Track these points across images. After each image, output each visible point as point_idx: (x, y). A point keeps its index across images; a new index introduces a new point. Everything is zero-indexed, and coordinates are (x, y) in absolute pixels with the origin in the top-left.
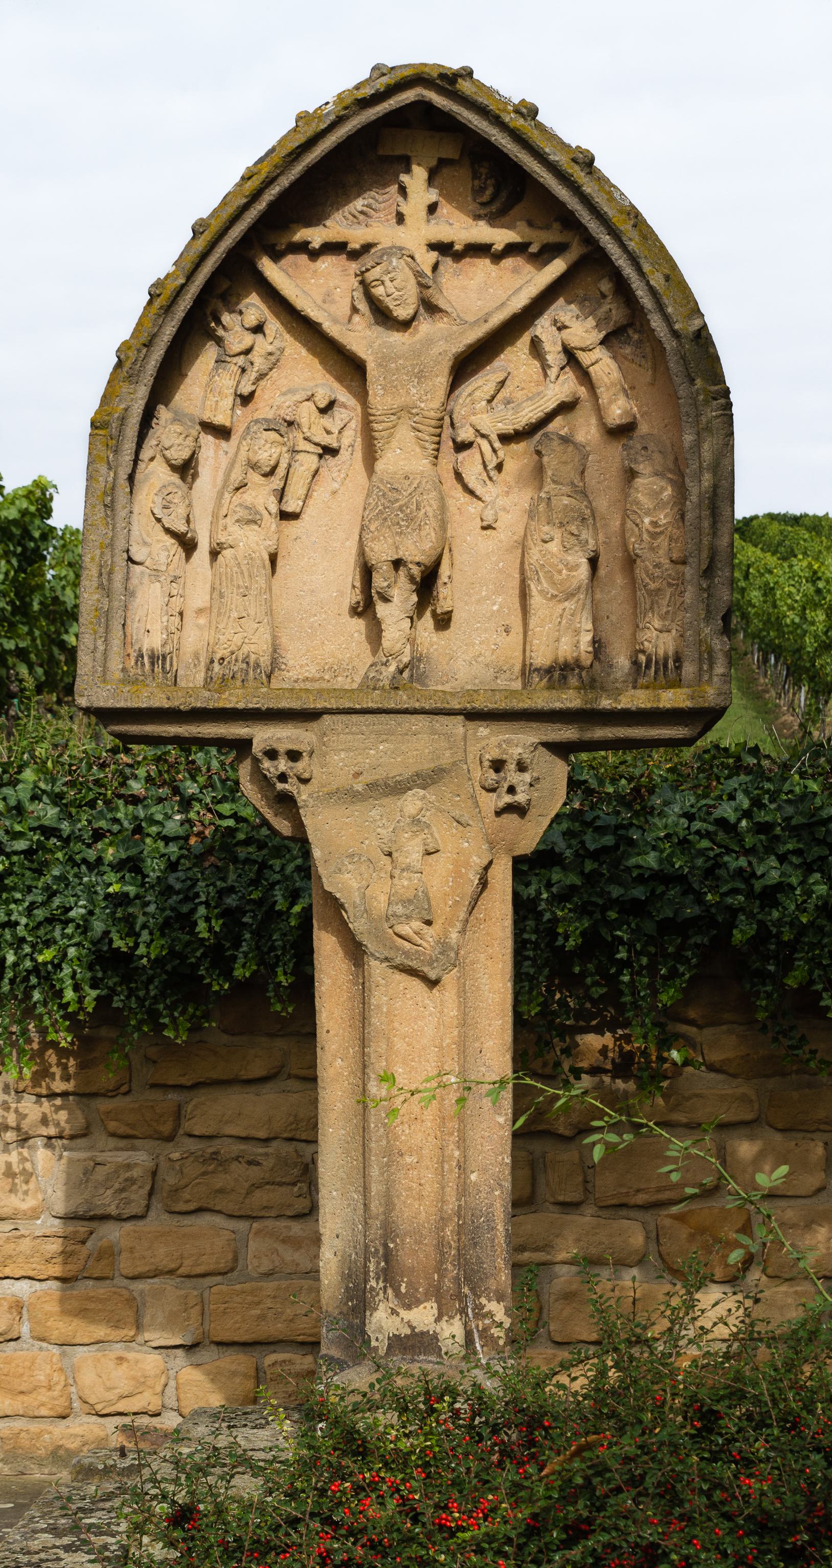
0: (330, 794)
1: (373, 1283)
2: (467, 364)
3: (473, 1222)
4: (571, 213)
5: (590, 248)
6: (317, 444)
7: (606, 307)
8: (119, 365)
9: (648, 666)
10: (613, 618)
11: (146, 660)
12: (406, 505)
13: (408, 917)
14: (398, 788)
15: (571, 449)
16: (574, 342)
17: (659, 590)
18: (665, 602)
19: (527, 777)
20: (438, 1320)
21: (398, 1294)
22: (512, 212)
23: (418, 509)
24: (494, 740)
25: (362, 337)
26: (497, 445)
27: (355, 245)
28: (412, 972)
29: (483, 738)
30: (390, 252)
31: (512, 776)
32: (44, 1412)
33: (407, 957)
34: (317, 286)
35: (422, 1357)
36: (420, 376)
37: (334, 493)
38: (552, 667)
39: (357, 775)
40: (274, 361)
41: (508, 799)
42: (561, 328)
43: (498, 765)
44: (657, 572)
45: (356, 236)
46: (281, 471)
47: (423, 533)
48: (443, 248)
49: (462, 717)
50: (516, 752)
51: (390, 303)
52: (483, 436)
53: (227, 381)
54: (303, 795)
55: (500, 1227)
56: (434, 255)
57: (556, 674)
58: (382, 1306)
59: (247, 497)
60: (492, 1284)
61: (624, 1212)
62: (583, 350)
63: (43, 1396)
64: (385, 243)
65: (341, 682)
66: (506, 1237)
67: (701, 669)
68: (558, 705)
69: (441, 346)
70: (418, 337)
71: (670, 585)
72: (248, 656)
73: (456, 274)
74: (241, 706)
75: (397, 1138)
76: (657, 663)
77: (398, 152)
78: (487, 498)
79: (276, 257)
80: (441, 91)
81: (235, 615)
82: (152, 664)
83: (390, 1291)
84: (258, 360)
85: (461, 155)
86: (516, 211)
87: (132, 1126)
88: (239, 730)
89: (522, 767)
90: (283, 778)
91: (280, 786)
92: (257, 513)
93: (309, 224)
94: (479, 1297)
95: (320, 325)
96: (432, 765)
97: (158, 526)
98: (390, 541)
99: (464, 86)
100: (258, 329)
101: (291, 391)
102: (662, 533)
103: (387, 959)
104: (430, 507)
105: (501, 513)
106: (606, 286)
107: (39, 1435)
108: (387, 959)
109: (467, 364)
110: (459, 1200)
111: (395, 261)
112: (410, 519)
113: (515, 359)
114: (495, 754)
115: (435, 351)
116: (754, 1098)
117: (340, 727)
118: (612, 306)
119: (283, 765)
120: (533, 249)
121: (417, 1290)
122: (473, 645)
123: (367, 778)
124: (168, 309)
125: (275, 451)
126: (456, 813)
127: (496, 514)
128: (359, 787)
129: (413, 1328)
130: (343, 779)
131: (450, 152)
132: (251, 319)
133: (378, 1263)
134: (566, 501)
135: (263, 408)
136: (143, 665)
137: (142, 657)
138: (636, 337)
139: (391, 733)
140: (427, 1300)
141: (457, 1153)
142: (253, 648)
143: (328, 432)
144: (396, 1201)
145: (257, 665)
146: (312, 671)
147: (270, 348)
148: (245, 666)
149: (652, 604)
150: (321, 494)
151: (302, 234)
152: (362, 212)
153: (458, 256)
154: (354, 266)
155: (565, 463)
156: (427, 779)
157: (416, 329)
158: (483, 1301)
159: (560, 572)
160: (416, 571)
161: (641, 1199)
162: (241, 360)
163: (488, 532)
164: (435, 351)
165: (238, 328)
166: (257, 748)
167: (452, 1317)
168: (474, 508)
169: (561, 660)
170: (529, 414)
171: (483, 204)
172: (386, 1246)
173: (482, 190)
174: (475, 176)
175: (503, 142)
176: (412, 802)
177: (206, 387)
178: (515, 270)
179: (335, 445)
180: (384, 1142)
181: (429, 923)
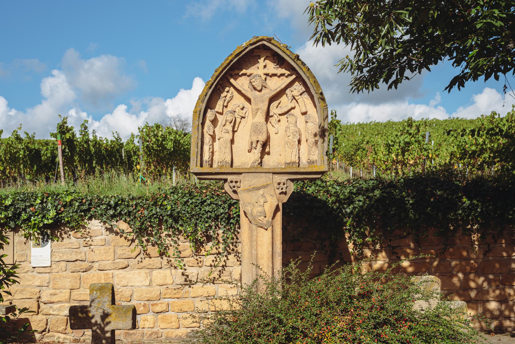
0: (244, 190)
2: (272, 100)
8: (199, 99)
14: (259, 189)
16: (294, 95)
19: (285, 186)
24: (278, 178)
25: (250, 94)
27: (248, 74)
28: (261, 227)
30: (256, 76)
31: (282, 185)
32: (174, 327)
34: (242, 83)
36: (263, 102)
40: (232, 98)
43: (279, 184)
45: (248, 72)
48: (267, 75)
50: (283, 181)
51: (256, 86)
54: (238, 190)
56: (265, 76)
59: (226, 127)
63: (173, 324)
64: (255, 74)
65: (245, 166)
68: (292, 171)
69: (267, 95)
73: (270, 80)
84: (228, 98)
86: (283, 66)
87: (193, 264)
90: (234, 187)
99: (273, 42)
100: (228, 92)
104: (265, 129)
107: (173, 332)
109: (272, 100)
113: (284, 99)
114: (279, 181)
120: (286, 75)
124: (210, 88)
126: (271, 194)
130: (247, 187)
135: (230, 108)
139: (257, 177)
146: (239, 164)
153: (271, 76)
154: (248, 78)
156: (264, 187)
160: (262, 143)
162: (224, 98)
164: (266, 96)
166: (229, 180)
168: (273, 129)
170: (285, 110)
176: (261, 192)
178: (282, 79)
181: (265, 217)
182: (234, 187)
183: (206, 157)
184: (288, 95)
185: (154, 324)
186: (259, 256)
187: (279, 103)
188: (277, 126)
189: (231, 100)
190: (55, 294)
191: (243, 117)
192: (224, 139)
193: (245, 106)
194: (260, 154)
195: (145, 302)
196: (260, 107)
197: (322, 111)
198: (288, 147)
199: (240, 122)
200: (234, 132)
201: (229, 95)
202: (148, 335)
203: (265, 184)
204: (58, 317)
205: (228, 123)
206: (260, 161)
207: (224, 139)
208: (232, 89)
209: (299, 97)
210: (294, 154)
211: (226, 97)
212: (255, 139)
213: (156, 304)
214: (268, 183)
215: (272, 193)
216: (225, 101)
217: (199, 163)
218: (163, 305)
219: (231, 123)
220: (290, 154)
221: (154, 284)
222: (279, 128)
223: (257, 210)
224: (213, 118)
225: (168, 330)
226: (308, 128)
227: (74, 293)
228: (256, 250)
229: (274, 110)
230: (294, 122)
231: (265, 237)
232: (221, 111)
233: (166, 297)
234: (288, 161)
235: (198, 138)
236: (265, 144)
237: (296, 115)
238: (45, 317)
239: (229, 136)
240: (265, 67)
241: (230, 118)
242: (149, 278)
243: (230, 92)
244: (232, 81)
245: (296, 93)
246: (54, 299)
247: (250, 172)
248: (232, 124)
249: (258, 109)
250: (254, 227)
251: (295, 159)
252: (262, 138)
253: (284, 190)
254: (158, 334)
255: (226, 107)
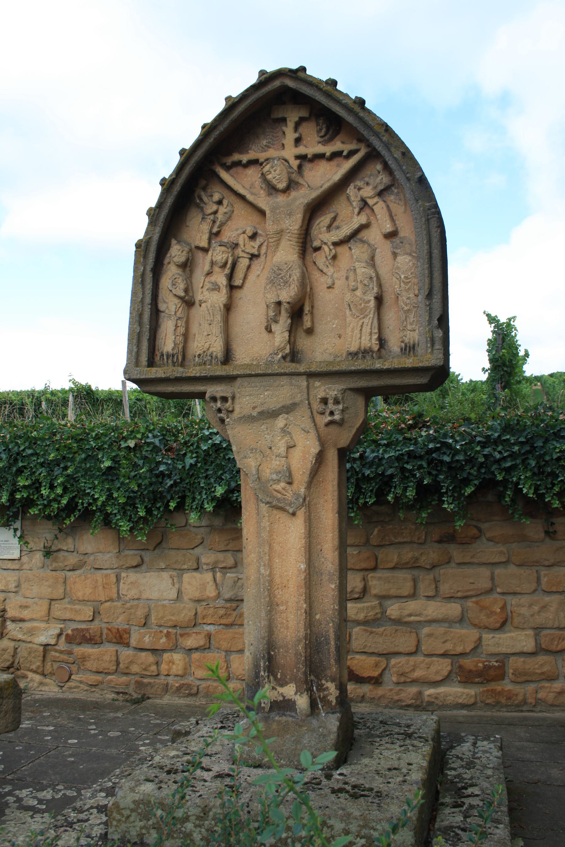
0: (240, 418)
1: (262, 673)
2: (315, 209)
3: (317, 640)
4: (356, 128)
5: (370, 149)
6: (248, 253)
7: (380, 178)
9: (405, 349)
10: (391, 328)
11: (165, 357)
12: (284, 276)
13: (279, 481)
14: (273, 414)
15: (366, 246)
17: (409, 310)
18: (412, 316)
19: (341, 407)
20: (296, 694)
21: (276, 678)
22: (335, 140)
23: (290, 277)
25: (263, 202)
26: (332, 247)
29: (317, 387)
33: (279, 502)
34: (245, 182)
35: (288, 713)
37: (258, 276)
38: (357, 352)
39: (254, 408)
41: (329, 418)
42: (359, 189)
43: (325, 401)
44: (408, 301)
45: (262, 156)
46: (229, 265)
47: (291, 288)
48: (302, 158)
49: (305, 377)
51: (275, 182)
52: (325, 244)
53: (205, 227)
55: (332, 643)
56: (298, 162)
57: (360, 355)
58: (267, 686)
59: (213, 278)
60: (329, 673)
61: (452, 600)
62: (370, 198)
66: (336, 648)
67: (427, 346)
69: (302, 200)
70: (290, 198)
71: (414, 307)
72: (212, 353)
73: (310, 170)
74: (198, 375)
75: (275, 596)
76: (410, 347)
77: (280, 116)
78: (329, 274)
79: (228, 168)
80: (291, 77)
81: (206, 334)
82: (168, 359)
83: (271, 678)
84: (220, 216)
85: (310, 115)
88: (199, 388)
89: (337, 402)
90: (219, 411)
91: (219, 415)
92: (217, 285)
93: (241, 153)
94: (321, 680)
95: (245, 196)
96: (291, 402)
97: (171, 294)
98: (275, 293)
100: (220, 203)
101: (237, 230)
102: (410, 282)
103: (268, 503)
105: (336, 281)
106: (379, 167)
108: (268, 503)
110: (306, 630)
111: (276, 162)
112: (286, 282)
115: (298, 203)
116: (506, 552)
117: (246, 384)
118: (383, 176)
119: (219, 404)
120: (345, 153)
121: (286, 677)
122: (324, 344)
123: (259, 410)
125: (225, 256)
126: (303, 426)
127: (334, 281)
128: (255, 414)
129: (284, 697)
130: (247, 411)
131: (304, 113)
132: (216, 197)
133: (265, 663)
134: (363, 270)
136: (163, 359)
137: (163, 355)
138: (396, 191)
140: (290, 683)
141: (305, 606)
142: (214, 349)
143: (254, 247)
144: (275, 629)
145: (216, 357)
146: (247, 361)
147: (225, 210)
148: (210, 358)
149: (406, 317)
150: (252, 277)
151: (236, 157)
152: (266, 146)
155: (363, 253)
156: (288, 409)
157: (289, 194)
158: (323, 682)
159: (361, 304)
161: (459, 594)
162: (212, 217)
163: (330, 290)
164: (298, 203)
165: (211, 203)
167: (302, 693)
168: (323, 279)
169: (362, 348)
170: (346, 231)
171: (322, 137)
172: (269, 653)
173: (321, 130)
174: (318, 125)
175: (322, 98)
176: (280, 422)
177: (197, 231)
179: (256, 253)
180: (268, 599)
181: (290, 483)
182: (219, 411)
183: (168, 341)
184: (352, 198)
185: (185, 669)
186: (277, 580)
187: (334, 219)
188: (330, 271)
189: (226, 222)
190: (27, 607)
191: (253, 257)
192: (209, 304)
193: (260, 232)
194: (286, 334)
195: (170, 630)
196: (284, 226)
197: (423, 219)
198: (353, 315)
199: (249, 267)
200: (232, 288)
201: (222, 210)
202: (174, 688)
203: (289, 402)
204: (30, 645)
205: (216, 269)
206: (287, 351)
207: (209, 304)
208: (229, 199)
209: (376, 200)
210: (366, 330)
211: (215, 213)
212: (272, 298)
213: (188, 635)
214: (297, 400)
215: (307, 423)
216: (214, 222)
217: (144, 358)
218: (199, 637)
219: (224, 265)
220: (357, 331)
221: (186, 598)
222: (335, 275)
223: (271, 467)
224: (183, 259)
225: (209, 683)
226: (398, 268)
227: (56, 606)
228: (270, 565)
229: (322, 235)
230: (366, 256)
231: (293, 532)
232: (204, 243)
233: (205, 621)
234: (353, 349)
235: (142, 301)
236: (297, 313)
237: (372, 242)
238: (12, 644)
239: (220, 298)
240: (298, 141)
241: (219, 254)
242: (177, 586)
243: (225, 202)
244: (224, 175)
245: (368, 192)
246: (25, 614)
247: (261, 375)
248: (227, 271)
249: (280, 233)
250: (264, 508)
251: (369, 341)
252: (287, 294)
253: (337, 417)
254: (191, 689)
255: (218, 234)
